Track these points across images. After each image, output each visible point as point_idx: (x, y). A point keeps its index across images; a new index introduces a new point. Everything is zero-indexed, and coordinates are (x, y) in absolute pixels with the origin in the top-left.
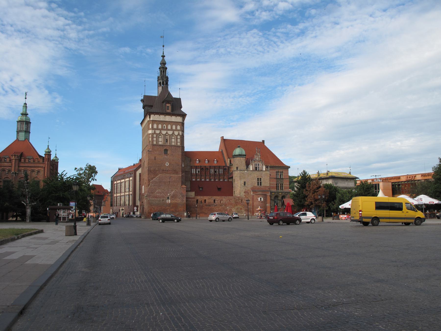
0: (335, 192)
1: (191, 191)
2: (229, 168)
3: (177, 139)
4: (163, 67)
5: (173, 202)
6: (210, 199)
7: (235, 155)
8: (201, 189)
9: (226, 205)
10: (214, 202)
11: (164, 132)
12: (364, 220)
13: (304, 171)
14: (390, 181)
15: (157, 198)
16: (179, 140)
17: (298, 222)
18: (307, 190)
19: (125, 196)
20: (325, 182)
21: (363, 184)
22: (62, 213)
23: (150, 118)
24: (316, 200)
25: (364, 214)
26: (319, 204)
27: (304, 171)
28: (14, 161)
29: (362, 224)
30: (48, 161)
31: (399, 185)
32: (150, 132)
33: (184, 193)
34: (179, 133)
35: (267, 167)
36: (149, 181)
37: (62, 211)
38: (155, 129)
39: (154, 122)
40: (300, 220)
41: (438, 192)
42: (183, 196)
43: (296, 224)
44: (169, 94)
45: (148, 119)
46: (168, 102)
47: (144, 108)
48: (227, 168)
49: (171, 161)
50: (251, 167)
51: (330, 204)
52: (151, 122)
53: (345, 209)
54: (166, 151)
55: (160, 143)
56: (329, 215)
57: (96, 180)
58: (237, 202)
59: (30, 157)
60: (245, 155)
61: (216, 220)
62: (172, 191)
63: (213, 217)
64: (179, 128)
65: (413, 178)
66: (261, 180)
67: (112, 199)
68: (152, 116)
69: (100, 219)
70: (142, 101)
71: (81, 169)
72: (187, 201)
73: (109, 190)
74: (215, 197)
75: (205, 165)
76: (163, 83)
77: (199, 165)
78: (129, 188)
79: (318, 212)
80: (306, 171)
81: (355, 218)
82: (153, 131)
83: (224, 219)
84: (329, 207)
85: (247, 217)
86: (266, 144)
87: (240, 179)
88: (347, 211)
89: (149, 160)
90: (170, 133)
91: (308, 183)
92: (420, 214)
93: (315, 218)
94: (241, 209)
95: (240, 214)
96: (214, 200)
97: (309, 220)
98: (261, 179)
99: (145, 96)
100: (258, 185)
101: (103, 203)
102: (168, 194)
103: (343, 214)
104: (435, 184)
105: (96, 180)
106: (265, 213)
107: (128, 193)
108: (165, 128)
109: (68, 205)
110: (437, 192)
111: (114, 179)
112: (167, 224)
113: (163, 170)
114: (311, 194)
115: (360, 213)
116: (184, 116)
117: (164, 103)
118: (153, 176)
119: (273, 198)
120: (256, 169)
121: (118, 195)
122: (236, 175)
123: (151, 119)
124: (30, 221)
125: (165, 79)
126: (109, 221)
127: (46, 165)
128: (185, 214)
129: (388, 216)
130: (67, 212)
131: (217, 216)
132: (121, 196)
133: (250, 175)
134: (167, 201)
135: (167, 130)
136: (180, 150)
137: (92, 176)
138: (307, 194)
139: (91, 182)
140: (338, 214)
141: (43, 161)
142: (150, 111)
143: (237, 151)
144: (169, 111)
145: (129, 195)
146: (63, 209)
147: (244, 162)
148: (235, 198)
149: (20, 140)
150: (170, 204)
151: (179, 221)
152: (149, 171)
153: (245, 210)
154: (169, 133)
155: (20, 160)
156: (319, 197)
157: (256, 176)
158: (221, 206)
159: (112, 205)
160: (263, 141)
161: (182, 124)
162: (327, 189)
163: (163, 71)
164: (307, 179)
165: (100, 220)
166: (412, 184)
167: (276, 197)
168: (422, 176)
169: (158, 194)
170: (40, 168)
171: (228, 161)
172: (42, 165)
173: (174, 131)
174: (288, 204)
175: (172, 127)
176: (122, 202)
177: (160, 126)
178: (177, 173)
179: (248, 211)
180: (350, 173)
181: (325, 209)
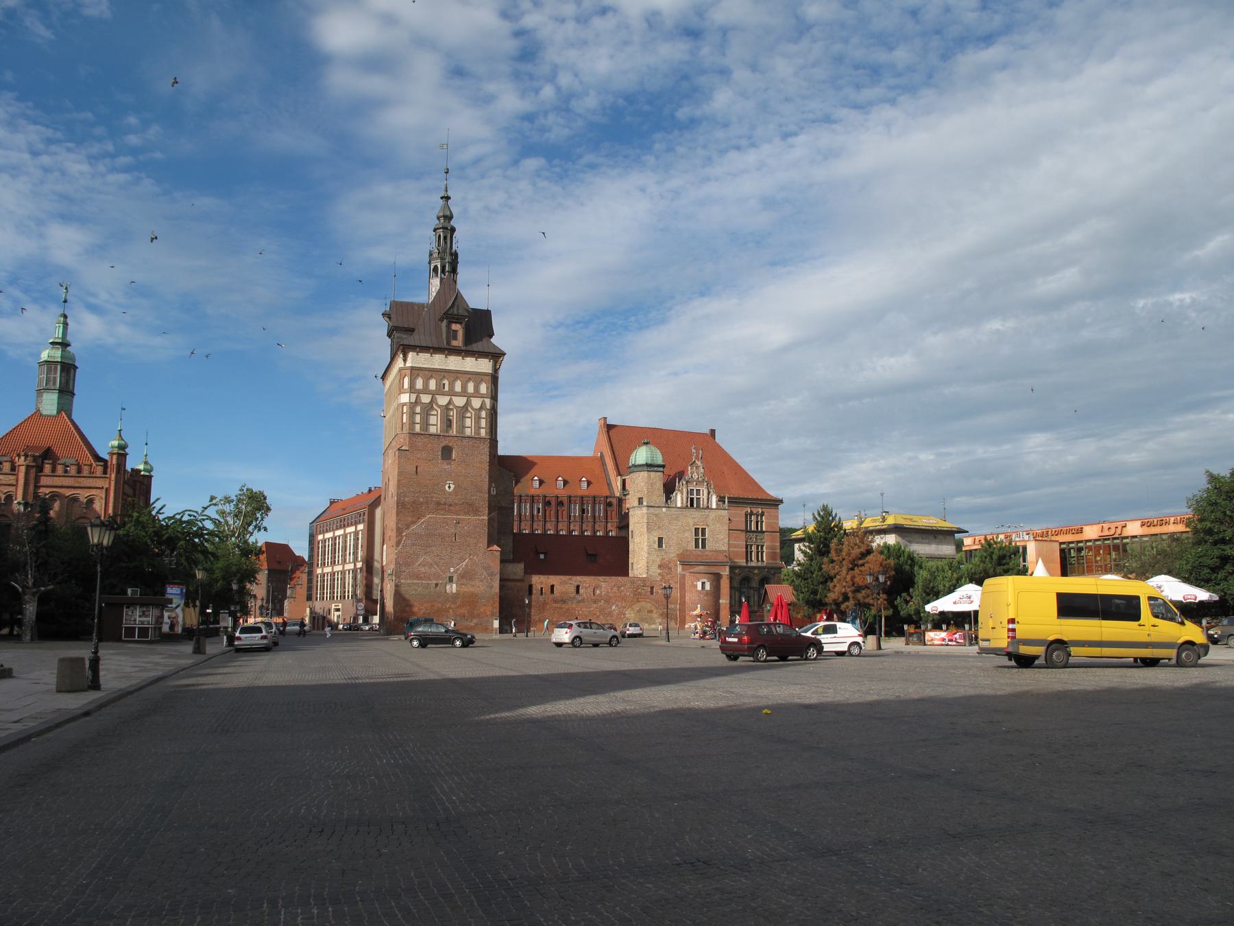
0: (912, 566)
1: (515, 561)
2: (621, 501)
3: (478, 418)
4: (446, 225)
5: (465, 589)
6: (565, 582)
8: (542, 556)
10: (578, 592)
11: (443, 400)
12: (1025, 650)
13: (825, 508)
14: (1054, 538)
15: (421, 578)
16: (483, 423)
17: (812, 653)
18: (832, 561)
19: (343, 572)
20: (878, 541)
21: (990, 545)
22: (136, 617)
23: (405, 360)
24: (858, 589)
25: (1022, 631)
26: (867, 601)
27: (825, 508)
28: (23, 469)
29: (1013, 663)
30: (118, 472)
31: (1080, 550)
32: (405, 398)
33: (496, 567)
34: (483, 403)
35: (721, 499)
36: (399, 531)
37: (138, 612)
38: (419, 392)
39: (415, 372)
40: (818, 645)
41: (1208, 567)
42: (491, 574)
43: (806, 659)
44: (458, 297)
45: (399, 363)
47: (389, 335)
48: (615, 502)
50: (679, 499)
51: (898, 601)
52: (408, 372)
53: (942, 613)
54: (447, 452)
55: (433, 430)
56: (895, 627)
57: (265, 529)
58: (640, 594)
59: (68, 461)
60: (663, 466)
61: (573, 642)
63: (564, 635)
64: (483, 389)
65: (1119, 531)
67: (310, 581)
68: (411, 355)
71: (228, 500)
72: (501, 587)
74: (579, 578)
75: (557, 492)
77: (540, 492)
78: (355, 553)
79: (864, 622)
80: (830, 507)
81: (993, 644)
82: (414, 396)
83: (596, 640)
84: (895, 608)
85: (664, 633)
86: (719, 439)
87: (649, 529)
88: (962, 621)
89: (400, 474)
90: (460, 401)
91: (835, 540)
92: (1192, 632)
93: (860, 640)
94: (650, 611)
95: (646, 626)
96: (578, 587)
97: (844, 648)
98: (704, 530)
99: (396, 305)
100: (697, 546)
101: (289, 592)
102: (452, 570)
103: (937, 627)
104: (1199, 543)
105: (265, 529)
106: (714, 623)
107: (351, 566)
108: (447, 388)
109: (163, 593)
110: (1201, 566)
112: (433, 651)
113: (438, 504)
114: (844, 572)
115: (1011, 626)
116: (496, 356)
119: (736, 584)
120: (692, 505)
122: (638, 519)
123: (409, 364)
124: (32, 639)
125: (448, 259)
126: (265, 641)
127: (113, 483)
128: (496, 624)
129: (1097, 638)
130: (153, 612)
131: (576, 631)
134: (448, 587)
135: (452, 393)
136: (487, 450)
138: (832, 573)
139: (251, 534)
140: (923, 627)
141: (105, 472)
142: (406, 342)
143: (641, 455)
145: (354, 571)
146: (142, 605)
148: (633, 582)
149: (44, 413)
150: (455, 597)
151: (468, 643)
152: (401, 505)
153: (661, 615)
155: (40, 469)
156: (869, 579)
157: (691, 522)
159: (309, 598)
160: (713, 432)
161: (494, 379)
162: (889, 557)
163: (445, 238)
164: (832, 529)
165: (239, 639)
166: (1116, 548)
167: (746, 580)
168: (1142, 525)
169: (423, 569)
170: (93, 492)
171: (617, 483)
172: (100, 483)
173: (469, 396)
174: (780, 599)
175: (464, 387)
176: (338, 591)
177: (432, 385)
178: (476, 512)
179: (667, 616)
181: (884, 613)
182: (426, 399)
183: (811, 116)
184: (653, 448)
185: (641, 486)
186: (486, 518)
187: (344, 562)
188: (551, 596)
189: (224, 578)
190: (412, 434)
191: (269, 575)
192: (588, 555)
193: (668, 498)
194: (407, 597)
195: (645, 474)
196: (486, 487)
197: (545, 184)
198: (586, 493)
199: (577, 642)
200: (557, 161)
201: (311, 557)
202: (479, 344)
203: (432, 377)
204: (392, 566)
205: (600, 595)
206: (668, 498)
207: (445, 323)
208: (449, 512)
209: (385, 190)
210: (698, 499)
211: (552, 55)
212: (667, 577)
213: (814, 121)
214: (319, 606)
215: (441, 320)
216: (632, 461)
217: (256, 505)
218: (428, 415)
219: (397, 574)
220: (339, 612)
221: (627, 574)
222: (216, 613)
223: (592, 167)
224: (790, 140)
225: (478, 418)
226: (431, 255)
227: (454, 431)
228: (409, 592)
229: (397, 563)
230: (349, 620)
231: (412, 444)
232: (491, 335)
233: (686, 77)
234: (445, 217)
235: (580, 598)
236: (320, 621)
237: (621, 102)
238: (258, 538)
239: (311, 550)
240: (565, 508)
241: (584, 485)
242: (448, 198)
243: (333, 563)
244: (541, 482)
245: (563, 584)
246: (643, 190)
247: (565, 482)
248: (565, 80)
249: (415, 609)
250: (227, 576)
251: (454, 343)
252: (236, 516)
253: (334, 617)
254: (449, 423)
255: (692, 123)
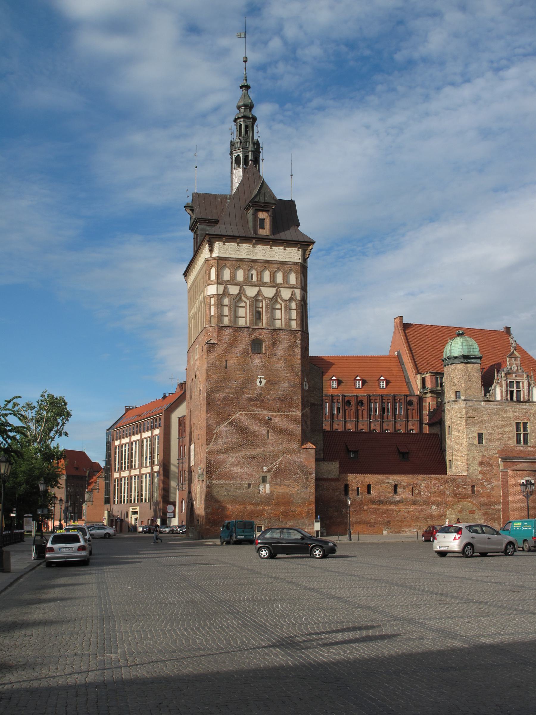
3: (288, 310)
5: (279, 489)
6: (382, 482)
7: (450, 358)
9: (428, 501)
10: (395, 491)
11: (251, 292)
16: (294, 314)
19: (140, 476)
23: (211, 250)
32: (212, 290)
33: (311, 466)
34: (293, 294)
36: (209, 429)
38: (226, 284)
39: (222, 262)
45: (205, 253)
46: (264, 207)
47: (192, 229)
48: (415, 400)
49: (273, 374)
50: (498, 392)
52: (215, 262)
54: (257, 344)
55: (242, 322)
57: (66, 434)
58: (460, 493)
60: (480, 358)
61: (463, 551)
62: (276, 458)
64: (293, 279)
66: (525, 429)
67: (108, 485)
68: (217, 245)
69: (49, 545)
70: (189, 207)
72: (317, 487)
73: (103, 464)
74: (396, 477)
76: (246, 157)
77: (336, 392)
78: (152, 457)
82: (221, 288)
87: (468, 425)
89: (209, 368)
90: (269, 292)
96: (396, 486)
98: (525, 424)
100: (518, 442)
101: (87, 496)
102: (265, 469)
105: (66, 434)
107: (148, 470)
108: (255, 279)
111: (115, 431)
113: (250, 399)
117: (251, 212)
118: (220, 416)
120: (512, 398)
121: (125, 474)
122: (454, 414)
123: (215, 254)
125: (251, 148)
126: (83, 553)
132: (130, 478)
133: (497, 413)
134: (261, 488)
135: (261, 284)
136: (298, 343)
137: (58, 424)
139: (53, 439)
142: (212, 232)
143: (456, 347)
144: (265, 231)
145: (151, 474)
147: (477, 378)
148: (453, 481)
150: (269, 498)
151: (329, 552)
152: (211, 402)
154: (266, 295)
157: (512, 416)
158: (414, 502)
159: (107, 501)
160: (508, 329)
163: (246, 127)
165: (51, 550)
169: (234, 469)
175: (273, 278)
176: (135, 494)
177: (240, 275)
178: (289, 408)
180: (356, 477)
182: (234, 290)
183: (521, 51)
184: (468, 339)
185: (456, 377)
186: (299, 414)
187: (141, 466)
188: (368, 496)
189: (27, 482)
190: (221, 327)
191: (68, 480)
192: (400, 453)
193: (487, 391)
194: (219, 498)
195: (462, 366)
196: (298, 381)
197: (280, 126)
198: (386, 392)
199: (468, 551)
200: (288, 106)
201: (108, 462)
202: (287, 232)
203: (239, 267)
204: (203, 466)
205: (419, 495)
206: (487, 391)
207: (251, 212)
208: (261, 408)
209: (138, 138)
210: (518, 392)
211: (480, 461)
212: (489, 475)
213: (525, 55)
214: (117, 509)
215: (247, 209)
216: (447, 353)
217: (56, 411)
218: (237, 307)
219: (209, 473)
220: (137, 516)
221: (444, 472)
222: (20, 517)
223: (321, 108)
224: (501, 73)
225: (288, 310)
226: (232, 145)
227: (264, 324)
228: (221, 494)
229: (208, 462)
230: (147, 522)
231: (220, 338)
232: (298, 225)
233: (400, 22)
234: (245, 106)
235: (397, 498)
236: (118, 523)
237: (344, 49)
238: (61, 444)
239: (108, 456)
240: (365, 407)
241: (383, 384)
242: (247, 87)
243: (130, 467)
244: (339, 382)
245: (380, 483)
246: (368, 127)
247: (364, 382)
248: (291, 32)
249: (228, 512)
250: (32, 480)
251: (262, 232)
252: (38, 421)
253: (132, 519)
254: (258, 315)
255: (410, 64)
